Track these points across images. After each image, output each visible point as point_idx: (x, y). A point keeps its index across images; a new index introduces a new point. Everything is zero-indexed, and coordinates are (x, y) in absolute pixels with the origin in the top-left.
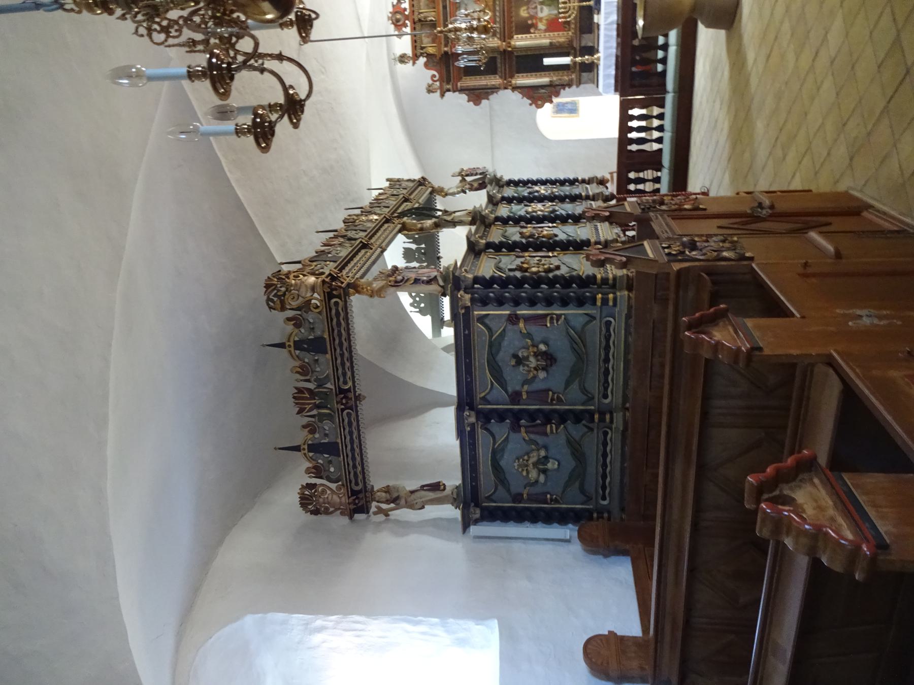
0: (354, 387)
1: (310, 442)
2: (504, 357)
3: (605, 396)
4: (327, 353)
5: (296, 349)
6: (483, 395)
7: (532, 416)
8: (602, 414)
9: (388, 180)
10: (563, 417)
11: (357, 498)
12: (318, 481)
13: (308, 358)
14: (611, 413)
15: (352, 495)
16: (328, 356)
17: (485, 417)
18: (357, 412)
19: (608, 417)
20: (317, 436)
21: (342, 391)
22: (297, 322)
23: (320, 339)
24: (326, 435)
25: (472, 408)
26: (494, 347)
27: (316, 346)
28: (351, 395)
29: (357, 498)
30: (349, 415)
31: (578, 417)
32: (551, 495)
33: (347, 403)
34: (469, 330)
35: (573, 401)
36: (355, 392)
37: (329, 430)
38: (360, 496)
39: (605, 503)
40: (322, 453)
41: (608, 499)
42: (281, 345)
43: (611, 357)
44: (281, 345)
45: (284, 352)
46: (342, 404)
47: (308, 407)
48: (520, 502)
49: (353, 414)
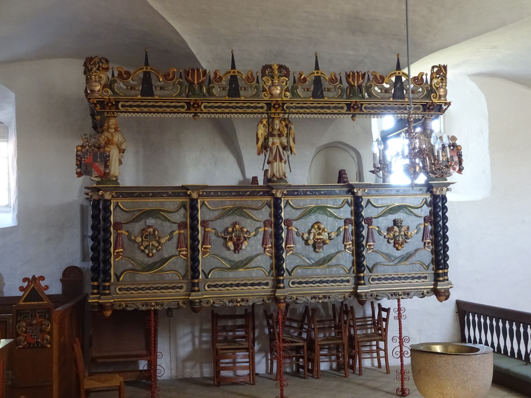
0: (363, 114)
5: (231, 76)
6: (206, 202)
9: (259, 154)
13: (224, 82)
16: (139, 97)
18: (345, 114)
19: (95, 291)
21: (117, 102)
22: (250, 79)
26: (323, 209)
30: (183, 107)
33: (194, 107)
36: (360, 114)
40: (143, 84)
45: (313, 69)
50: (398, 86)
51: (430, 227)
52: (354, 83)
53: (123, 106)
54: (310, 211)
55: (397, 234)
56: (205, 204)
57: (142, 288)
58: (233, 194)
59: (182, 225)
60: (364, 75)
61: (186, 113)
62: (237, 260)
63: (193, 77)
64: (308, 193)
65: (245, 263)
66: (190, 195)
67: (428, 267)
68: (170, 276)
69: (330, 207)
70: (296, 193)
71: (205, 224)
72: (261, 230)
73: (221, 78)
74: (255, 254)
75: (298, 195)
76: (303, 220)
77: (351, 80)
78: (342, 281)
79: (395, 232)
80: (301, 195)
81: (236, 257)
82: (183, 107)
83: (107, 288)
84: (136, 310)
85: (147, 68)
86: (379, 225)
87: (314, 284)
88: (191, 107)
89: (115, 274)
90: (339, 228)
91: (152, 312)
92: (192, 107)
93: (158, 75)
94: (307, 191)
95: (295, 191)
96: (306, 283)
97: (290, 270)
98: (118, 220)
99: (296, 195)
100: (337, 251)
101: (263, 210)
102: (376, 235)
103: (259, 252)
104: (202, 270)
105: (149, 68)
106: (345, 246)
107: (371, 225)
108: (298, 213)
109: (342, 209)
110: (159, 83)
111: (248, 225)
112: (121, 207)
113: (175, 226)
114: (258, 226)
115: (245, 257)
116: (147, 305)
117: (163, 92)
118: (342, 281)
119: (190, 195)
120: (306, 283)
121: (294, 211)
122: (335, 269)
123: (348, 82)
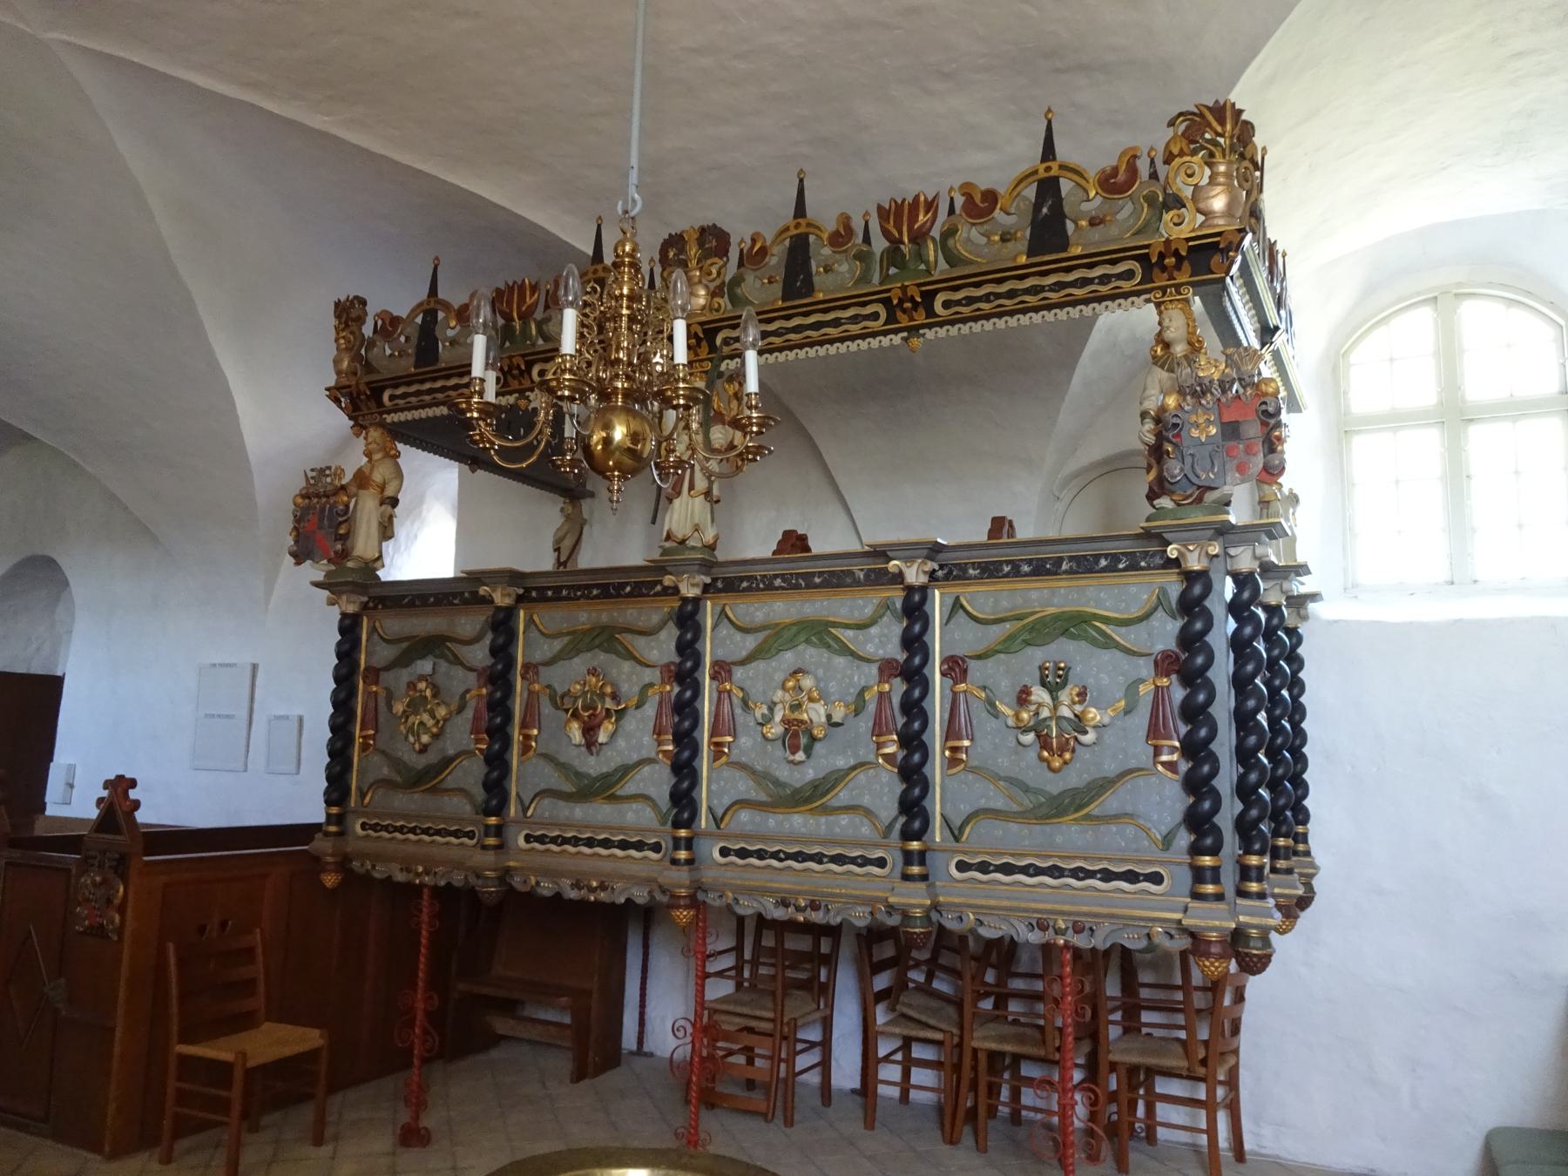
1: (812, 238)
2: (1064, 650)
3: (962, 866)
4: (784, 300)
7: (914, 708)
8: (689, 844)
10: (913, 774)
11: (916, 305)
12: (734, 254)
14: (924, 878)
15: (922, 294)
16: (1023, 260)
17: (503, 625)
20: (827, 251)
21: (929, 297)
22: (1114, 183)
23: (809, 288)
24: (828, 269)
25: (520, 599)
27: (1048, 228)
28: (920, 317)
29: (368, 397)
31: (913, 808)
32: (373, 737)
33: (1164, 269)
34: (434, 604)
35: (525, 775)
37: (835, 275)
38: (372, 404)
39: (521, 842)
41: (529, 846)
42: (800, 209)
43: (846, 867)
44: (800, 209)
46: (901, 301)
47: (891, 227)
48: (713, 678)
49: (1126, 285)
50: (1045, 210)
51: (1178, 694)
52: (901, 233)
53: (392, 398)
54: (1041, 630)
55: (1045, 713)
56: (962, 607)
57: (402, 827)
58: (595, 592)
59: (888, 669)
60: (931, 205)
61: (885, 333)
62: (593, 773)
63: (510, 303)
64: (778, 582)
65: (603, 788)
66: (899, 577)
67: (1167, 841)
68: (1117, 844)
69: (1107, 620)
70: (745, 584)
71: (722, 670)
72: (1146, 690)
73: (764, 251)
74: (635, 757)
75: (749, 589)
76: (760, 665)
77: (891, 227)
78: (865, 862)
79: (1040, 705)
80: (758, 589)
81: (593, 766)
82: (1129, 275)
83: (1208, 874)
84: (558, 896)
85: (1048, 169)
86: (989, 683)
87: (781, 860)
88: (1156, 271)
89: (359, 789)
90: (468, 691)
91: (426, 894)
92: (1206, 259)
93: (1083, 182)
94: (776, 576)
95: (742, 579)
96: (761, 855)
97: (720, 813)
98: (721, 654)
99: (745, 590)
100: (852, 762)
101: (663, 635)
102: (980, 713)
103: (645, 754)
104: (518, 795)
105: (1054, 165)
106: (1157, 751)
107: (964, 680)
108: (751, 642)
109: (874, 630)
110: (1085, 207)
111: (629, 678)
112: (969, 608)
113: (1145, 668)
114: (647, 680)
115: (613, 765)
116: (1043, 927)
117: (1096, 234)
118: (865, 862)
119: (1176, 563)
120: (761, 855)
121: (738, 636)
122: (844, 820)
123: (886, 233)
